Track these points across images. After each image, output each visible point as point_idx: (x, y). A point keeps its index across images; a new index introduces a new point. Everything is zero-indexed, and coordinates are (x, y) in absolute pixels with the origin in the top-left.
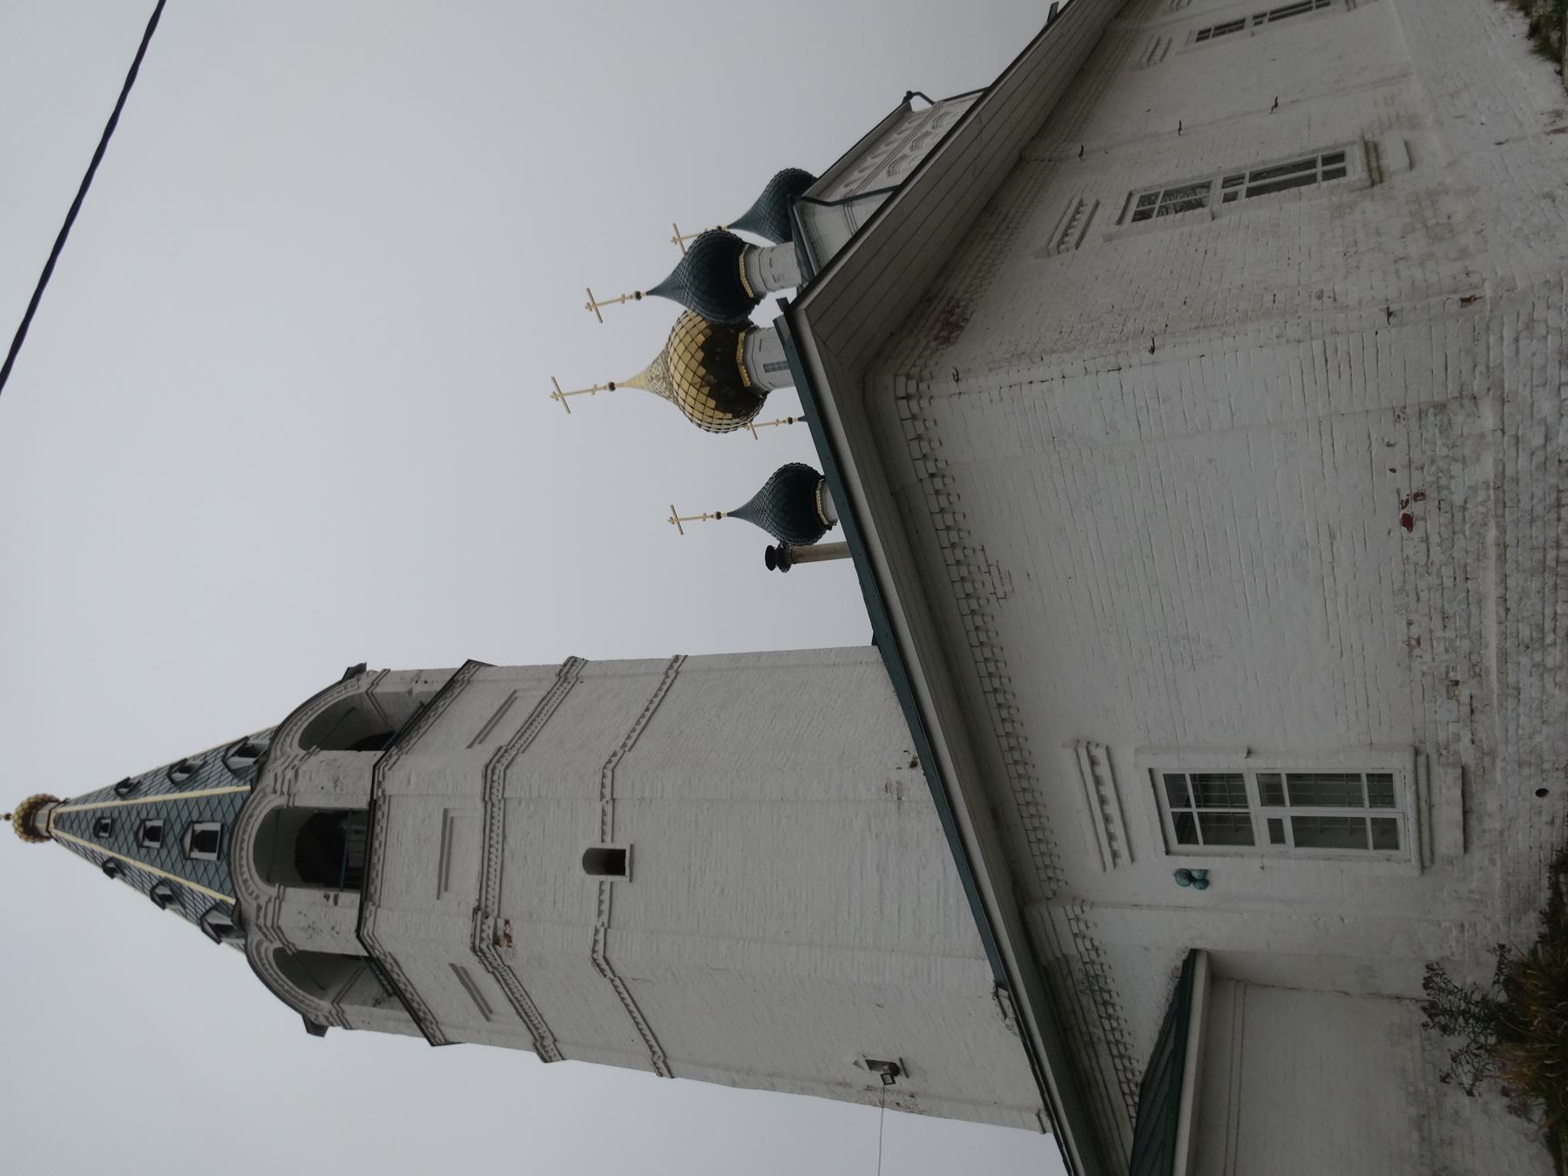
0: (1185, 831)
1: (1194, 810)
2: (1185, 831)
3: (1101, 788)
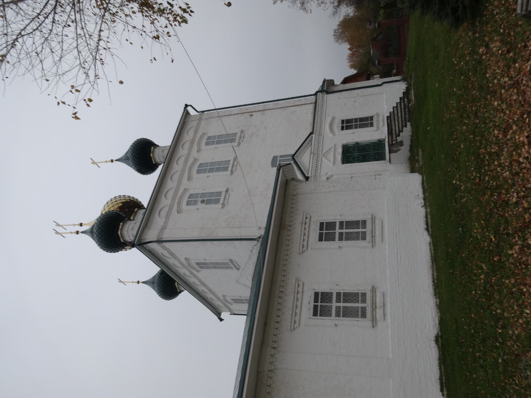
0: (315, 314)
1: (319, 304)
2: (315, 314)
3: (299, 288)
